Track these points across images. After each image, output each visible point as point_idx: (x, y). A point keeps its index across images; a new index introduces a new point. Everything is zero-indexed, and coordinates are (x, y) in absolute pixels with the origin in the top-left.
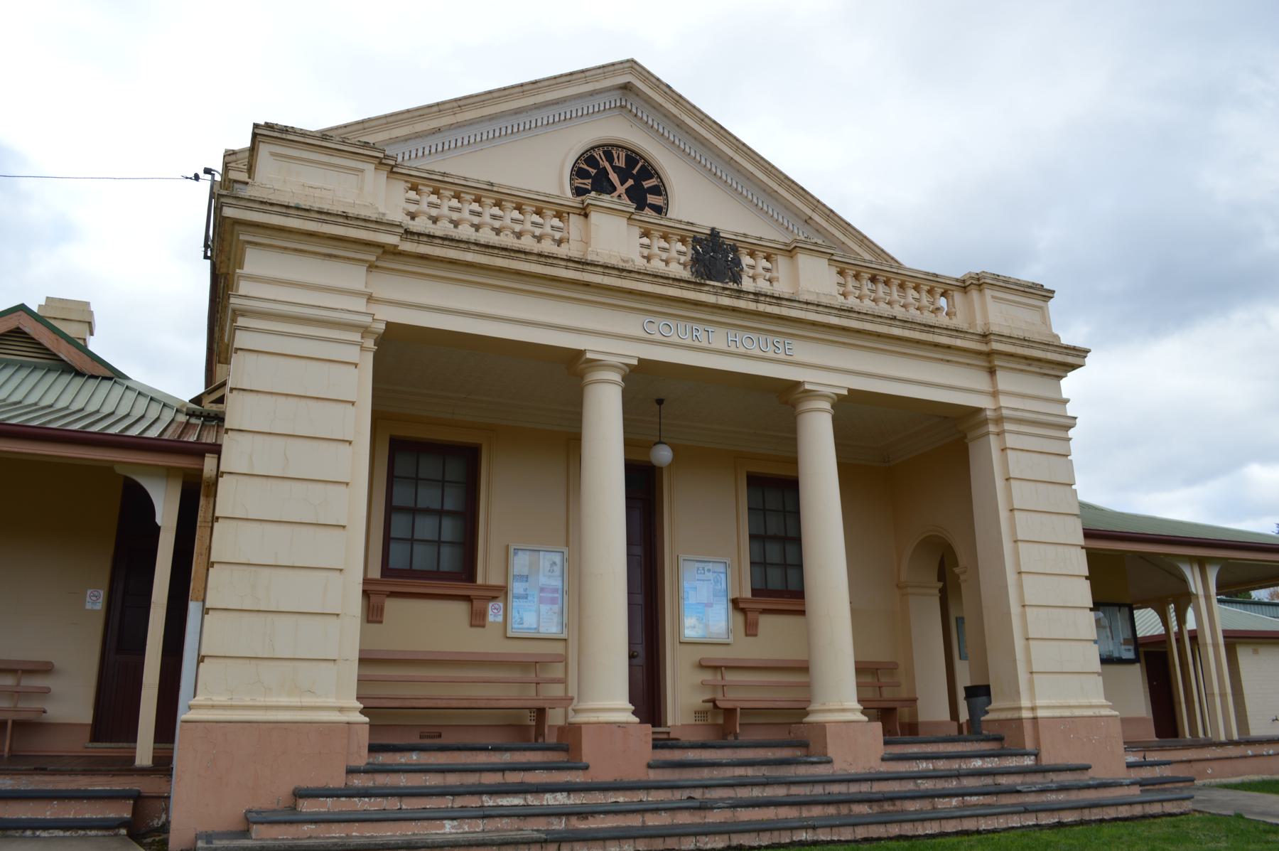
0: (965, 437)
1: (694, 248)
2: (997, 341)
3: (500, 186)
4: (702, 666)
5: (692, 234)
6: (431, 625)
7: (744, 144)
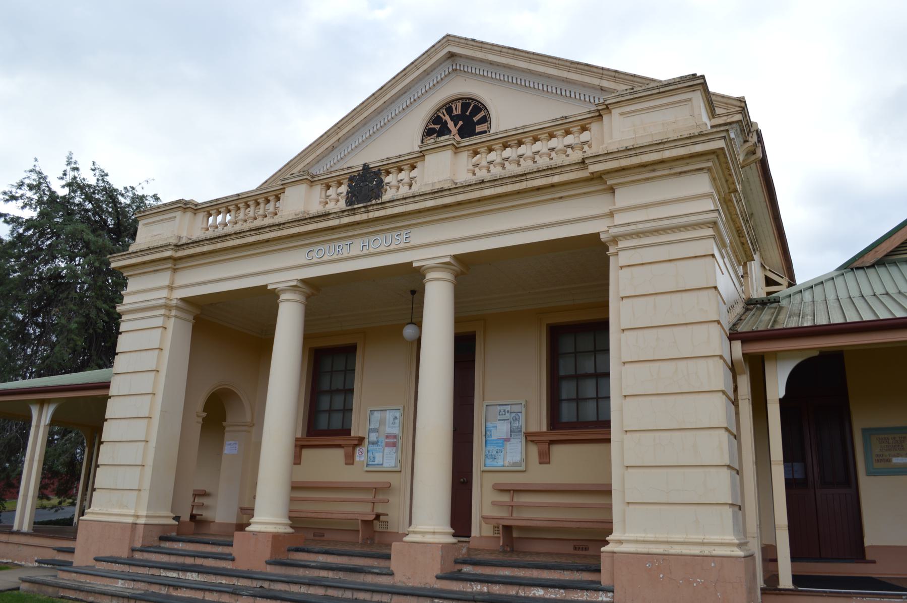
2: (594, 163)
3: (243, 194)
4: (502, 489)
5: (348, 176)
6: (327, 464)
7: (534, 54)
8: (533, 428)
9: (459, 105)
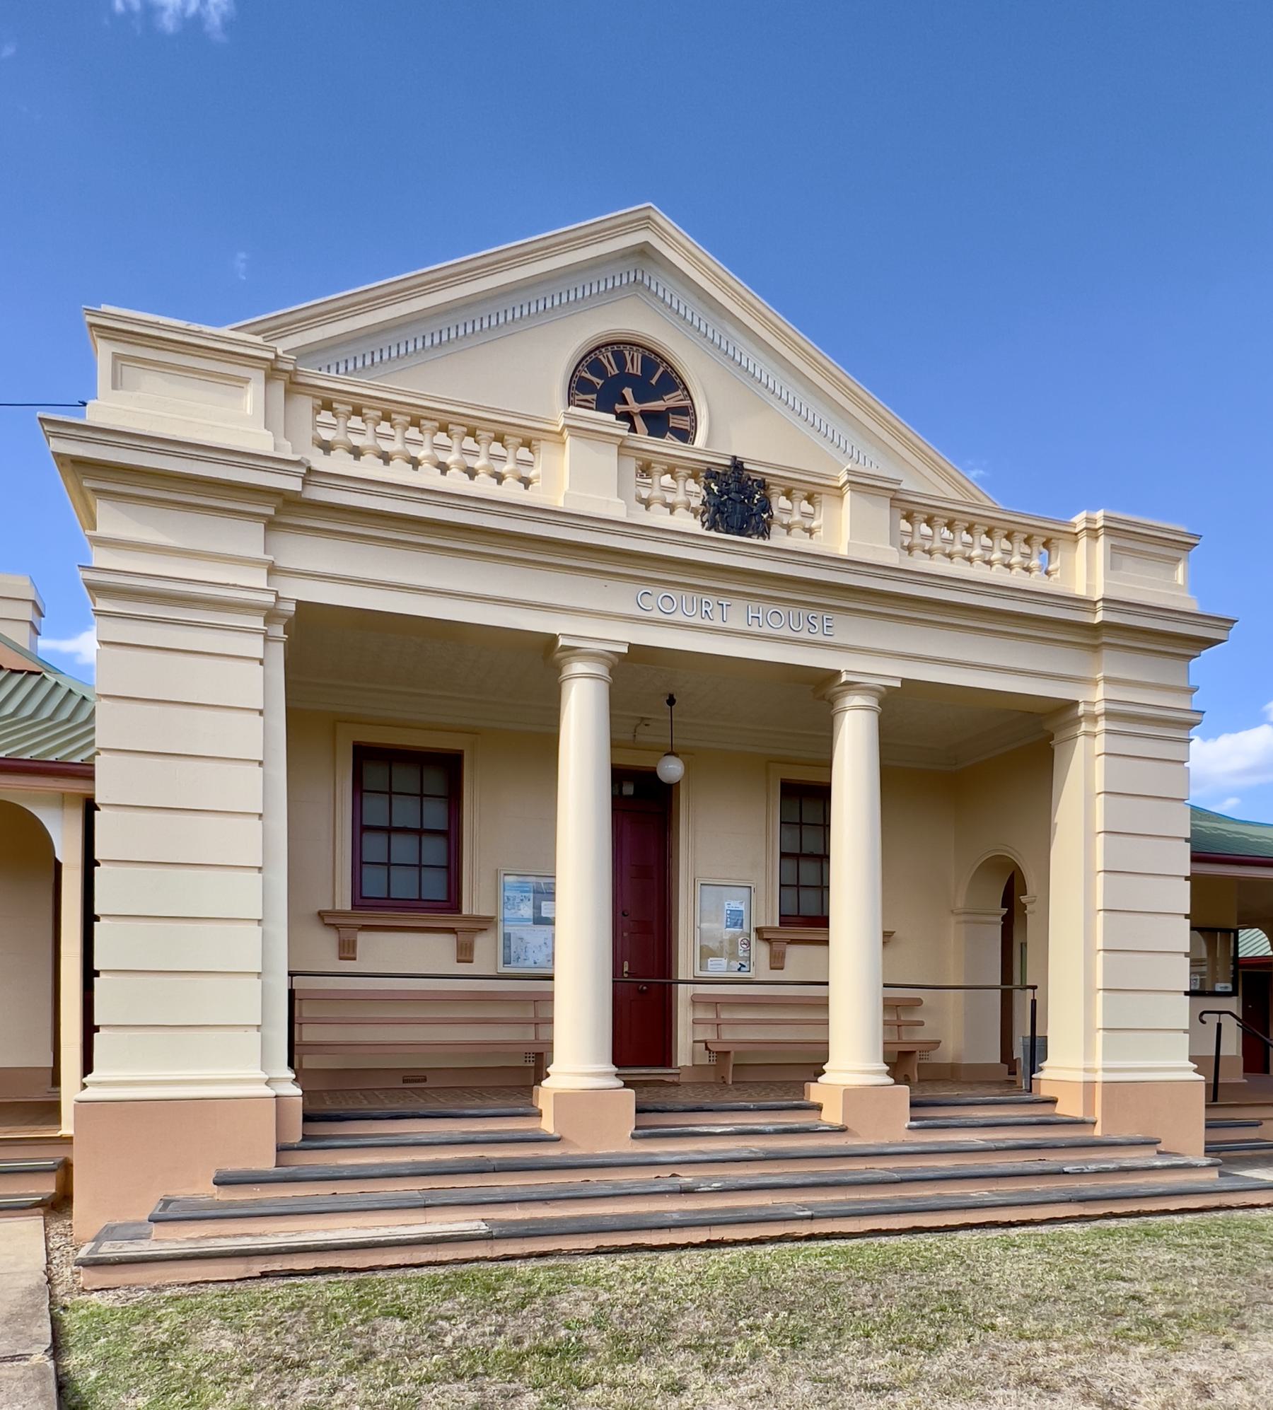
0: (1052, 738)
1: (708, 488)
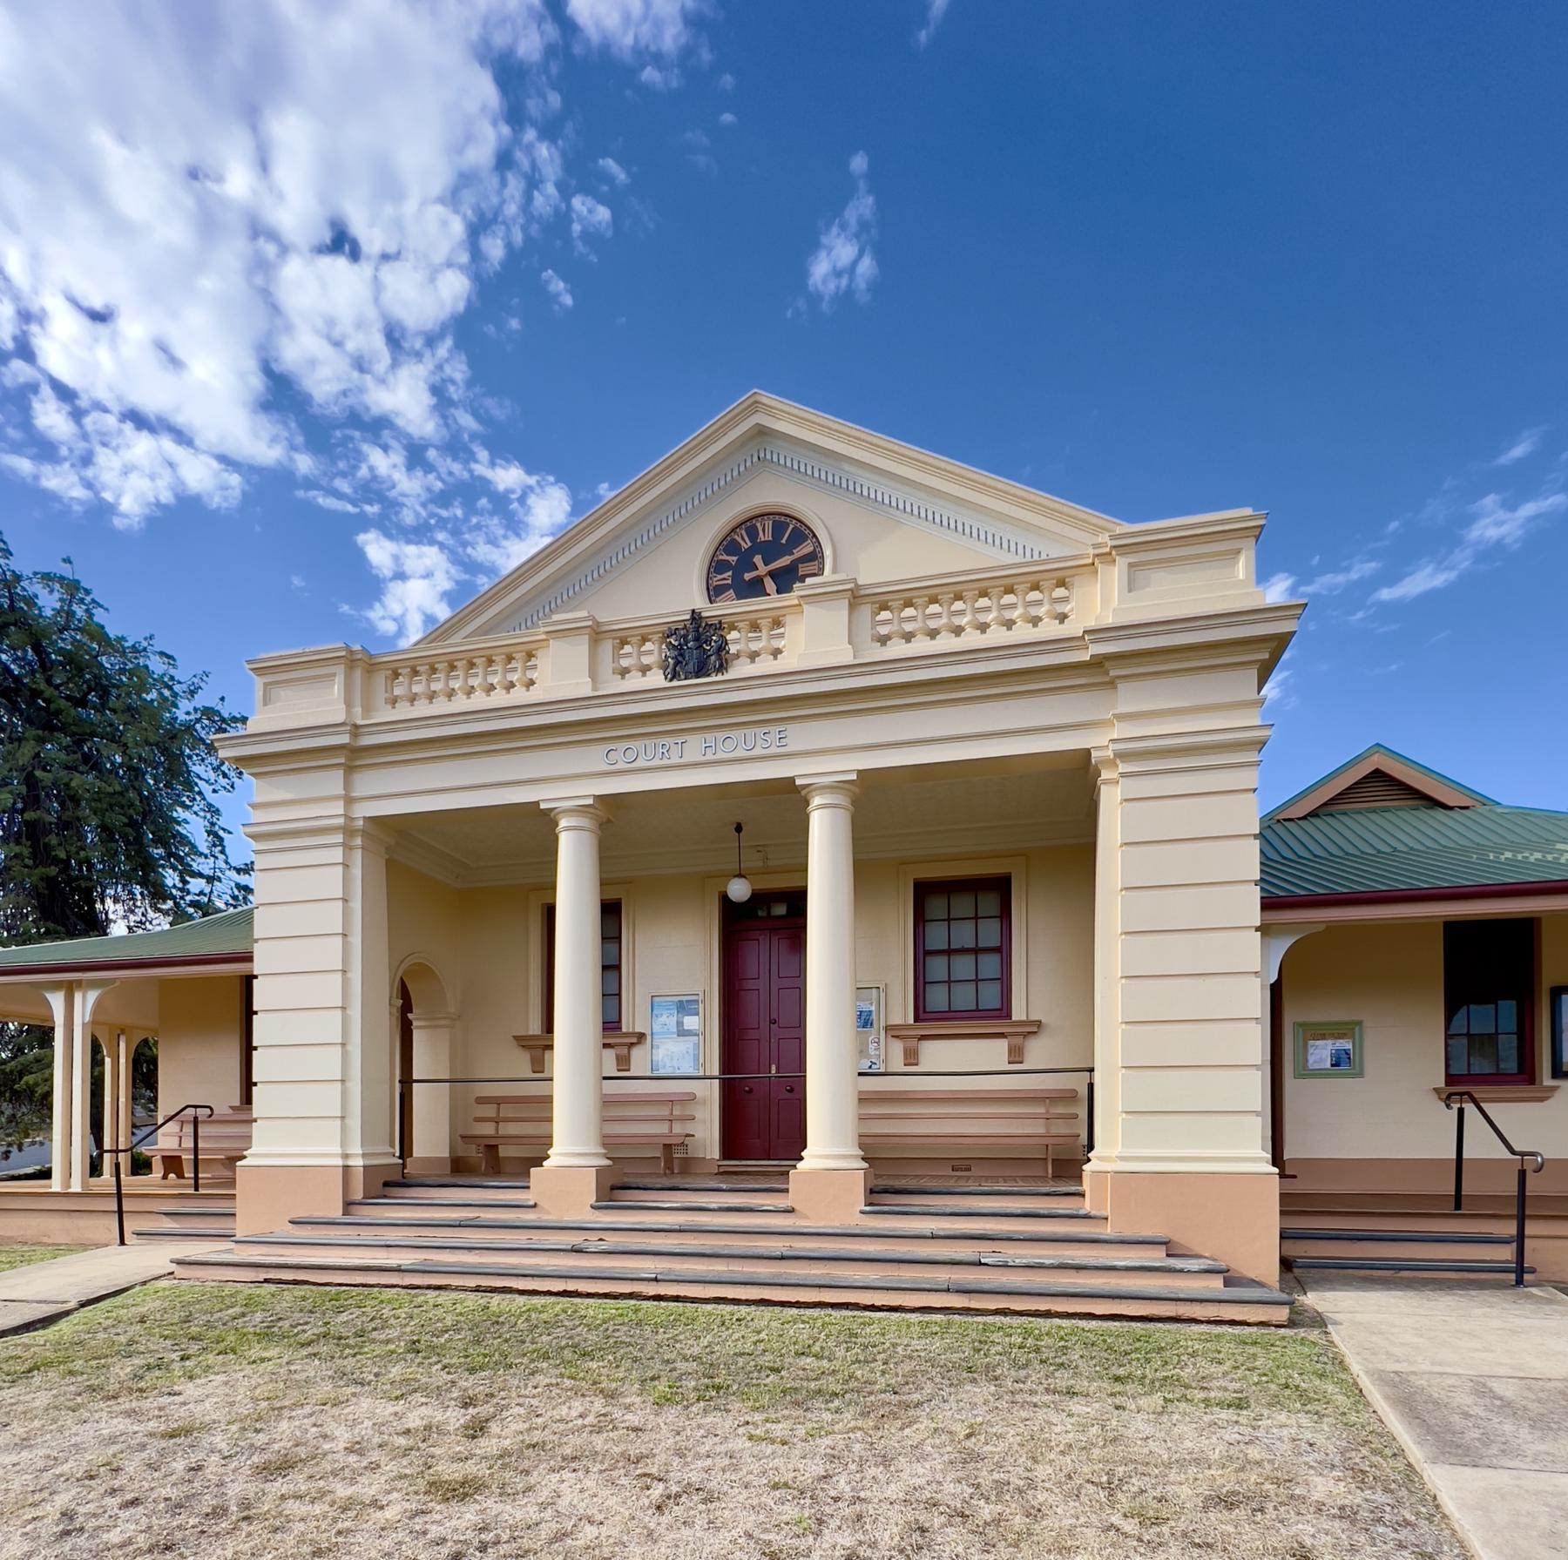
5: (665, 628)
8: (897, 1019)
9: (769, 524)
